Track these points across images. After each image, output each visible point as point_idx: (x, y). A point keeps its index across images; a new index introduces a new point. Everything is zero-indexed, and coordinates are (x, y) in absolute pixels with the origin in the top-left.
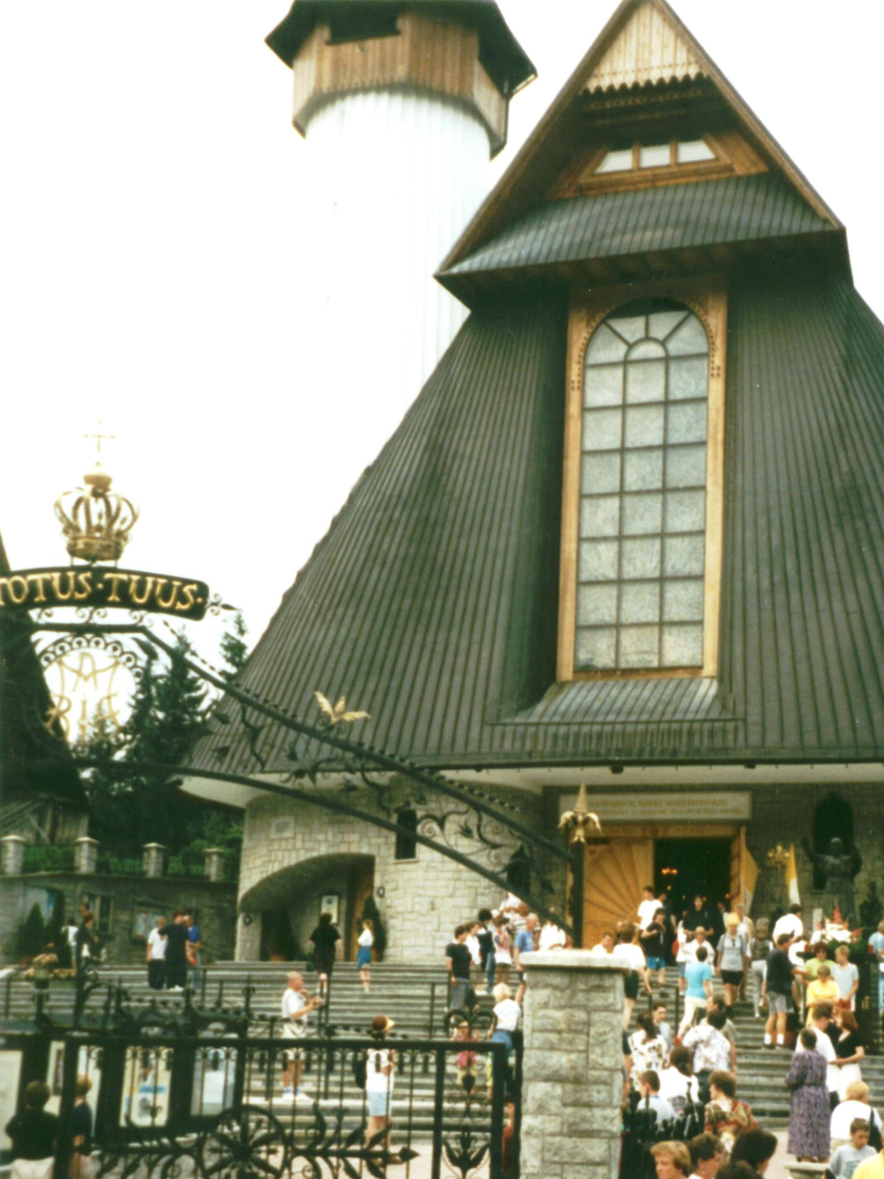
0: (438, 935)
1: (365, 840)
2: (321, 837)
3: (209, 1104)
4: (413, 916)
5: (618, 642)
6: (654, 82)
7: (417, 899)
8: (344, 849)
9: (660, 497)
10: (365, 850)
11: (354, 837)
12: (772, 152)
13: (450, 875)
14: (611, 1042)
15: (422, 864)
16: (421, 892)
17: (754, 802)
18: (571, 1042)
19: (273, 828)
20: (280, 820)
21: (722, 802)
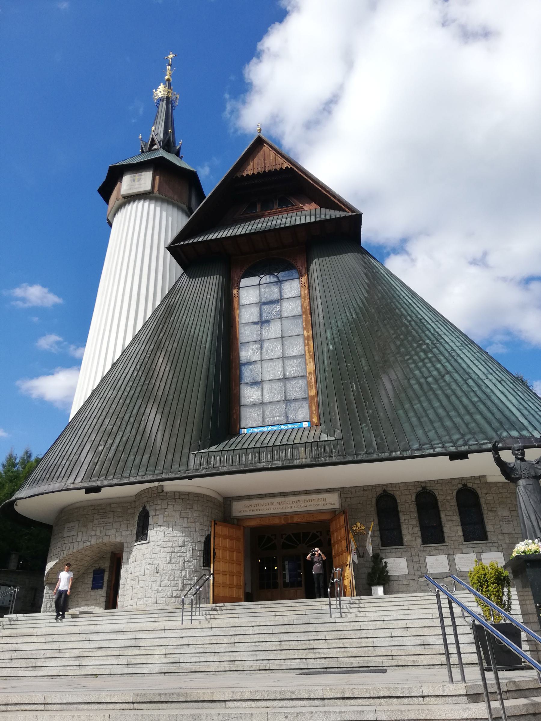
0: (160, 589)
1: (119, 533)
2: (93, 533)
3: (377, 590)
4: (144, 578)
5: (263, 411)
6: (267, 171)
7: (148, 567)
8: (106, 540)
9: (282, 384)
10: (118, 540)
11: (113, 532)
12: (293, 514)
13: (168, 550)
14: (316, 556)
15: (151, 544)
16: (150, 562)
17: (341, 498)
18: (408, 522)
19: (66, 530)
20: (71, 525)
21: (323, 499)
